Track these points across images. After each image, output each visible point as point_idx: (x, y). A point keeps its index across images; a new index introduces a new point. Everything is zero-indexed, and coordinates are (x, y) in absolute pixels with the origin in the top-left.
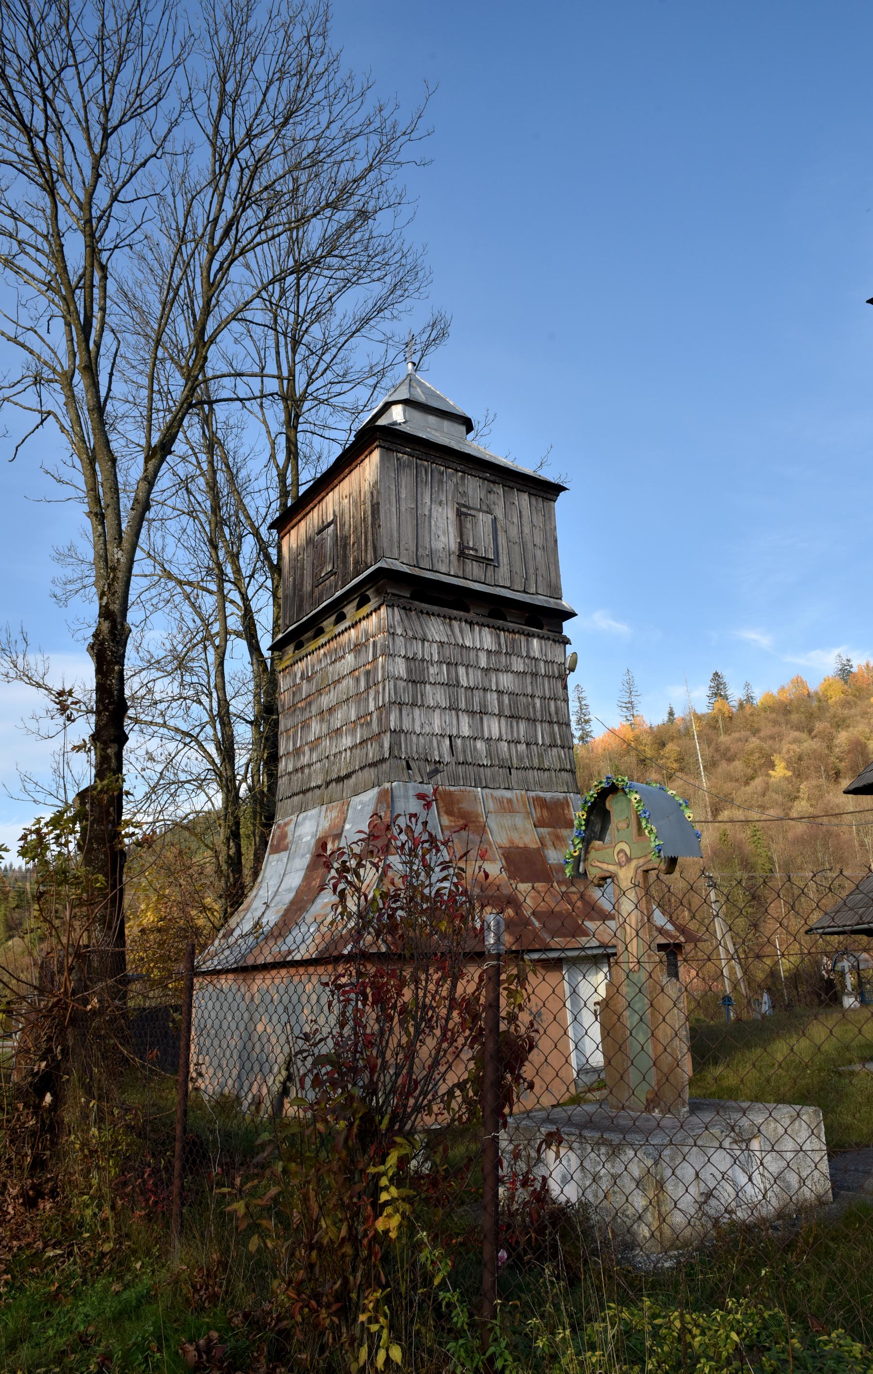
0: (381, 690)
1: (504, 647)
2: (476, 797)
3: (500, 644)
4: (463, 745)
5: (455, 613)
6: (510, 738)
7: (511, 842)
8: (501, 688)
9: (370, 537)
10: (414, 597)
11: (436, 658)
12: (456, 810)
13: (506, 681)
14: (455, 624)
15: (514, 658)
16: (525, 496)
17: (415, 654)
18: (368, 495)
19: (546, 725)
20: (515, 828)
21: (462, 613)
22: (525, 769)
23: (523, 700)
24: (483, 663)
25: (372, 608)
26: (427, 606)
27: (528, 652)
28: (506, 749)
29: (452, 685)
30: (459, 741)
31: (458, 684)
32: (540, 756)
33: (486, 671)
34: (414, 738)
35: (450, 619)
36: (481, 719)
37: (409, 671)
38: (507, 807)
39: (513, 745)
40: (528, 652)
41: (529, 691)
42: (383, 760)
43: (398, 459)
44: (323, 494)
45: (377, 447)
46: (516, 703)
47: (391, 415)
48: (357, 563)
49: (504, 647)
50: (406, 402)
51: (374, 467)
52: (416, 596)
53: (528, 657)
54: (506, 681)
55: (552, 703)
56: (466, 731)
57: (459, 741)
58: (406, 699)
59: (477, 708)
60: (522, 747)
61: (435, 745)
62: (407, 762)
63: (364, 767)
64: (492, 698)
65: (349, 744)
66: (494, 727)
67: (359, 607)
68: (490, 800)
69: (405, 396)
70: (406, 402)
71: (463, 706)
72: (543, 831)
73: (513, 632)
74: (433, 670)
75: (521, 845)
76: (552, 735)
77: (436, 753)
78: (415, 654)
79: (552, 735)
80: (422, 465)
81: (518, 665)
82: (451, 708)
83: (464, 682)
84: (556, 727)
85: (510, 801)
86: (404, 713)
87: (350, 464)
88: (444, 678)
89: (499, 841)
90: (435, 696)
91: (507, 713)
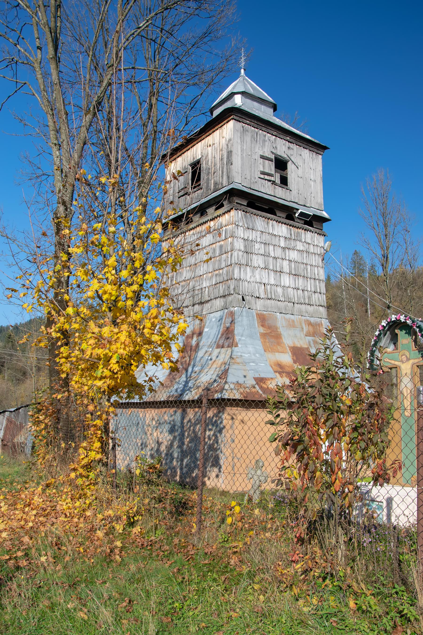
0: (229, 256)
1: (293, 236)
2: (276, 318)
3: (291, 234)
4: (271, 288)
5: (269, 215)
6: (294, 287)
7: (294, 343)
8: (291, 259)
9: (225, 170)
10: (249, 205)
11: (259, 240)
12: (266, 324)
13: (293, 255)
14: (271, 222)
15: (298, 242)
16: (307, 151)
17: (248, 237)
18: (225, 146)
19: (312, 281)
20: (296, 336)
21: (272, 216)
22: (301, 304)
23: (302, 266)
24: (282, 244)
25: (226, 210)
26: (254, 211)
27: (305, 239)
28: (292, 293)
29: (266, 255)
30: (269, 287)
31: (269, 256)
32: (309, 298)
33: (284, 249)
34: (246, 283)
35: (268, 219)
36: (280, 275)
37: (245, 247)
38: (291, 325)
39: (295, 290)
40: (305, 239)
41: (305, 262)
42: (230, 294)
43: (243, 127)
44: (195, 143)
45: (232, 119)
46: (298, 267)
47: (234, 100)
48: (216, 184)
49: (293, 236)
50: (243, 93)
51: (229, 131)
52: (250, 205)
53: (305, 242)
54: (293, 255)
55: (316, 268)
56: (272, 282)
57: (269, 287)
58: (244, 262)
59: (278, 269)
60: (300, 292)
61: (257, 288)
62: (243, 297)
63: (217, 298)
64: (286, 264)
65: (208, 285)
66: (286, 280)
67: (216, 209)
68: (283, 320)
69: (242, 90)
70: (243, 93)
71: (271, 267)
72: (310, 338)
73: (298, 228)
74: (257, 246)
75: (299, 346)
76: (315, 286)
77: (257, 292)
78: (248, 237)
79: (315, 286)
80: (254, 131)
81: (300, 246)
82: (265, 268)
83: (272, 254)
84: (317, 281)
85: (293, 321)
86: (242, 270)
87: (214, 127)
88: (262, 251)
89: (288, 343)
90: (258, 261)
91: (293, 272)
